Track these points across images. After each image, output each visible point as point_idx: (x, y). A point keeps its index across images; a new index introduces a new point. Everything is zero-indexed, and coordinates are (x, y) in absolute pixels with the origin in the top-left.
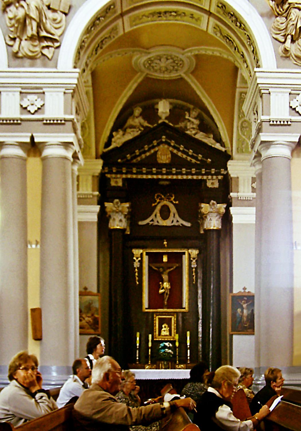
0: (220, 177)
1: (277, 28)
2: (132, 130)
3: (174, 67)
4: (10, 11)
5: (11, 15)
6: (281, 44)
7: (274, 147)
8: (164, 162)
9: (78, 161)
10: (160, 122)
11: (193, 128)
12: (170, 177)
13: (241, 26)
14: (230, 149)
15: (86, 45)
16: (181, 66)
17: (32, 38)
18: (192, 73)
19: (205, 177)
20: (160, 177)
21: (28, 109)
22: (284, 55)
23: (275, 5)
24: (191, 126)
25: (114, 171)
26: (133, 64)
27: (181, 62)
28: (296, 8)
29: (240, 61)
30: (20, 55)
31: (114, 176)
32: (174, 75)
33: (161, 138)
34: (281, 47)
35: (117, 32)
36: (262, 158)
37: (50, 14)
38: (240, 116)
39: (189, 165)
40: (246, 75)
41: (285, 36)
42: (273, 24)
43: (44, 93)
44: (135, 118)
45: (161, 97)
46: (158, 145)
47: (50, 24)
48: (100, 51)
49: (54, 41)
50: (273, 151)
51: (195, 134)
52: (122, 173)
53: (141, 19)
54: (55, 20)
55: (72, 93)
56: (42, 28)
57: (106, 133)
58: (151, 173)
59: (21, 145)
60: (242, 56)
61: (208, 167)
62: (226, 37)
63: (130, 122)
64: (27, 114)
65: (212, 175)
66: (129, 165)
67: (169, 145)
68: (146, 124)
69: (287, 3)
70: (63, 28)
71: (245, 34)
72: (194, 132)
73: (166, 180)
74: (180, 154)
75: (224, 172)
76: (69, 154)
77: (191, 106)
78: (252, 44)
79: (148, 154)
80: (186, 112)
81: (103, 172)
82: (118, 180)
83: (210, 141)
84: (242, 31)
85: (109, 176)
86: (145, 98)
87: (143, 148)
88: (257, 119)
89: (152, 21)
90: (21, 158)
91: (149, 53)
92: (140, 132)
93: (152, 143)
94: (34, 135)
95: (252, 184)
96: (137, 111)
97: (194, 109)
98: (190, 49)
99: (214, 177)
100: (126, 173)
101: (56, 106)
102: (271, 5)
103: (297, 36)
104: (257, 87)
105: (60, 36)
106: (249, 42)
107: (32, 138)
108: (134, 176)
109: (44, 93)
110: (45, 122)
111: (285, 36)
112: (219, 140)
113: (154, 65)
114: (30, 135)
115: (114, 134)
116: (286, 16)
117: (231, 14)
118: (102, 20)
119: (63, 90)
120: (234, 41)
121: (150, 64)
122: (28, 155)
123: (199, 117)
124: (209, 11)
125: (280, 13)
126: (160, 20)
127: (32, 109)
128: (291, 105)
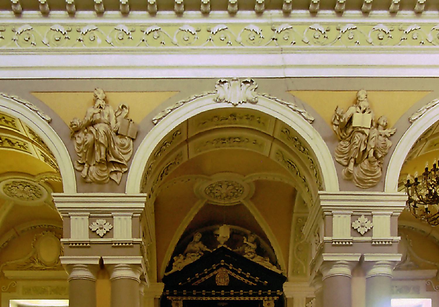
0: (276, 298)
1: (340, 151)
2: (193, 254)
3: (234, 193)
4: (78, 137)
5: (79, 141)
6: (344, 167)
7: (337, 267)
8: (223, 285)
11: (251, 252)
12: (228, 299)
13: (304, 150)
14: (286, 272)
15: (153, 170)
16: (241, 192)
17: (100, 163)
18: (251, 199)
19: (261, 299)
20: (219, 298)
21: (98, 232)
22: (346, 178)
23: (338, 129)
24: (249, 252)
26: (195, 192)
27: (241, 188)
28: (359, 132)
29: (302, 185)
30: (89, 180)
31: (174, 298)
32: (234, 201)
34: (344, 171)
35: (182, 158)
36: (323, 278)
37: (118, 140)
38: (296, 240)
39: (247, 287)
40: (306, 198)
41: (348, 160)
42: (336, 148)
44: (195, 243)
45: (221, 222)
46: (217, 268)
47: (118, 149)
48: (165, 177)
49: (121, 165)
50: (336, 270)
51: (253, 258)
52: (182, 295)
53: (205, 145)
54: (123, 145)
55: (139, 217)
56: (110, 153)
57: (167, 258)
59: (90, 267)
60: (303, 181)
61: (265, 288)
62: (288, 162)
63: (190, 247)
65: (269, 296)
66: (189, 288)
67: (228, 268)
68: (206, 249)
69: (351, 127)
70: (131, 153)
71: (309, 158)
72: (251, 256)
73: (224, 301)
74: (238, 277)
75: (280, 293)
76: (138, 277)
77: (248, 232)
78: (315, 168)
79: (207, 277)
81: (165, 294)
82: (178, 302)
83: (267, 264)
84: (306, 155)
85: (169, 298)
86: (205, 225)
87: (203, 271)
88: (318, 241)
89: (216, 147)
90: (88, 279)
91: (210, 180)
92: (200, 256)
93: (211, 266)
94: (103, 257)
95: (306, 304)
96: (197, 237)
97: (252, 233)
98: (252, 175)
99: (270, 298)
100: (187, 296)
101: (123, 230)
102: (335, 129)
103: (360, 160)
104: (320, 209)
105: (127, 162)
106: (312, 166)
107: (101, 260)
108: (194, 298)
111: (348, 160)
112: (275, 263)
113: (215, 191)
114: (100, 257)
115: (175, 258)
116: (350, 140)
117: (295, 139)
118: (168, 145)
120: (296, 166)
121: (211, 191)
122: (98, 277)
123: (256, 242)
124: (273, 136)
125: (344, 137)
126: (224, 146)
127: (101, 233)
128: (353, 226)
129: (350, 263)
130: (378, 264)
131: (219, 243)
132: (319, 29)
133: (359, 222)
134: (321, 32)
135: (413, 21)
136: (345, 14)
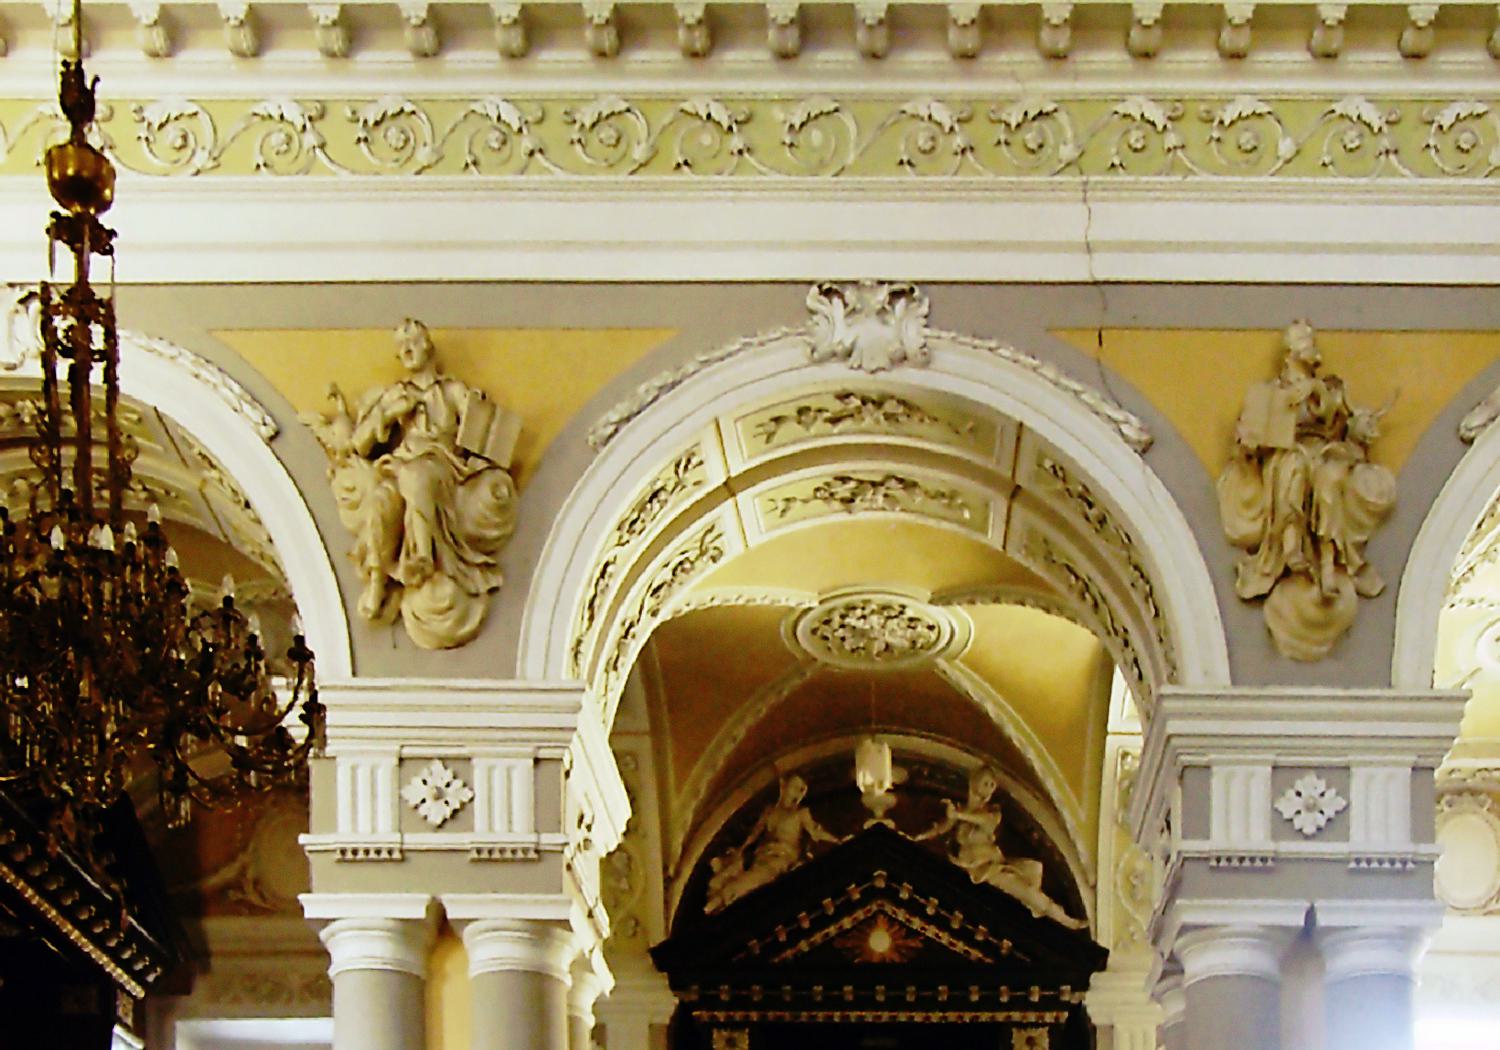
9: (588, 975)
10: (868, 825)
24: (980, 858)
25: (910, 998)
31: (721, 1016)
33: (870, 878)
43: (1207, 767)
58: (963, 1004)
64: (1293, 839)
80: (944, 801)
90: (1258, 979)
107: (1310, 915)
109: (1207, 767)
110: (1353, 865)
114: (1307, 905)
115: (716, 863)
119: (1271, 757)
127: (1308, 823)
129: (1269, 935)
130: (1224, 936)
131: (871, 814)
132: (1365, 118)
133: (1299, 794)
134: (1153, 124)
135: (1130, 85)
136: (1254, 62)
